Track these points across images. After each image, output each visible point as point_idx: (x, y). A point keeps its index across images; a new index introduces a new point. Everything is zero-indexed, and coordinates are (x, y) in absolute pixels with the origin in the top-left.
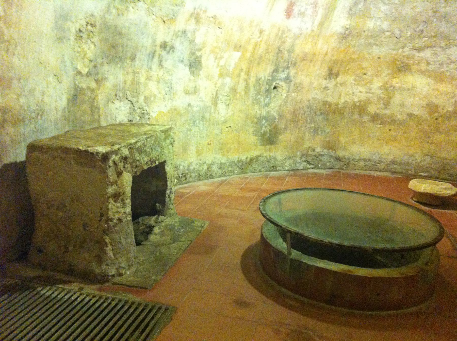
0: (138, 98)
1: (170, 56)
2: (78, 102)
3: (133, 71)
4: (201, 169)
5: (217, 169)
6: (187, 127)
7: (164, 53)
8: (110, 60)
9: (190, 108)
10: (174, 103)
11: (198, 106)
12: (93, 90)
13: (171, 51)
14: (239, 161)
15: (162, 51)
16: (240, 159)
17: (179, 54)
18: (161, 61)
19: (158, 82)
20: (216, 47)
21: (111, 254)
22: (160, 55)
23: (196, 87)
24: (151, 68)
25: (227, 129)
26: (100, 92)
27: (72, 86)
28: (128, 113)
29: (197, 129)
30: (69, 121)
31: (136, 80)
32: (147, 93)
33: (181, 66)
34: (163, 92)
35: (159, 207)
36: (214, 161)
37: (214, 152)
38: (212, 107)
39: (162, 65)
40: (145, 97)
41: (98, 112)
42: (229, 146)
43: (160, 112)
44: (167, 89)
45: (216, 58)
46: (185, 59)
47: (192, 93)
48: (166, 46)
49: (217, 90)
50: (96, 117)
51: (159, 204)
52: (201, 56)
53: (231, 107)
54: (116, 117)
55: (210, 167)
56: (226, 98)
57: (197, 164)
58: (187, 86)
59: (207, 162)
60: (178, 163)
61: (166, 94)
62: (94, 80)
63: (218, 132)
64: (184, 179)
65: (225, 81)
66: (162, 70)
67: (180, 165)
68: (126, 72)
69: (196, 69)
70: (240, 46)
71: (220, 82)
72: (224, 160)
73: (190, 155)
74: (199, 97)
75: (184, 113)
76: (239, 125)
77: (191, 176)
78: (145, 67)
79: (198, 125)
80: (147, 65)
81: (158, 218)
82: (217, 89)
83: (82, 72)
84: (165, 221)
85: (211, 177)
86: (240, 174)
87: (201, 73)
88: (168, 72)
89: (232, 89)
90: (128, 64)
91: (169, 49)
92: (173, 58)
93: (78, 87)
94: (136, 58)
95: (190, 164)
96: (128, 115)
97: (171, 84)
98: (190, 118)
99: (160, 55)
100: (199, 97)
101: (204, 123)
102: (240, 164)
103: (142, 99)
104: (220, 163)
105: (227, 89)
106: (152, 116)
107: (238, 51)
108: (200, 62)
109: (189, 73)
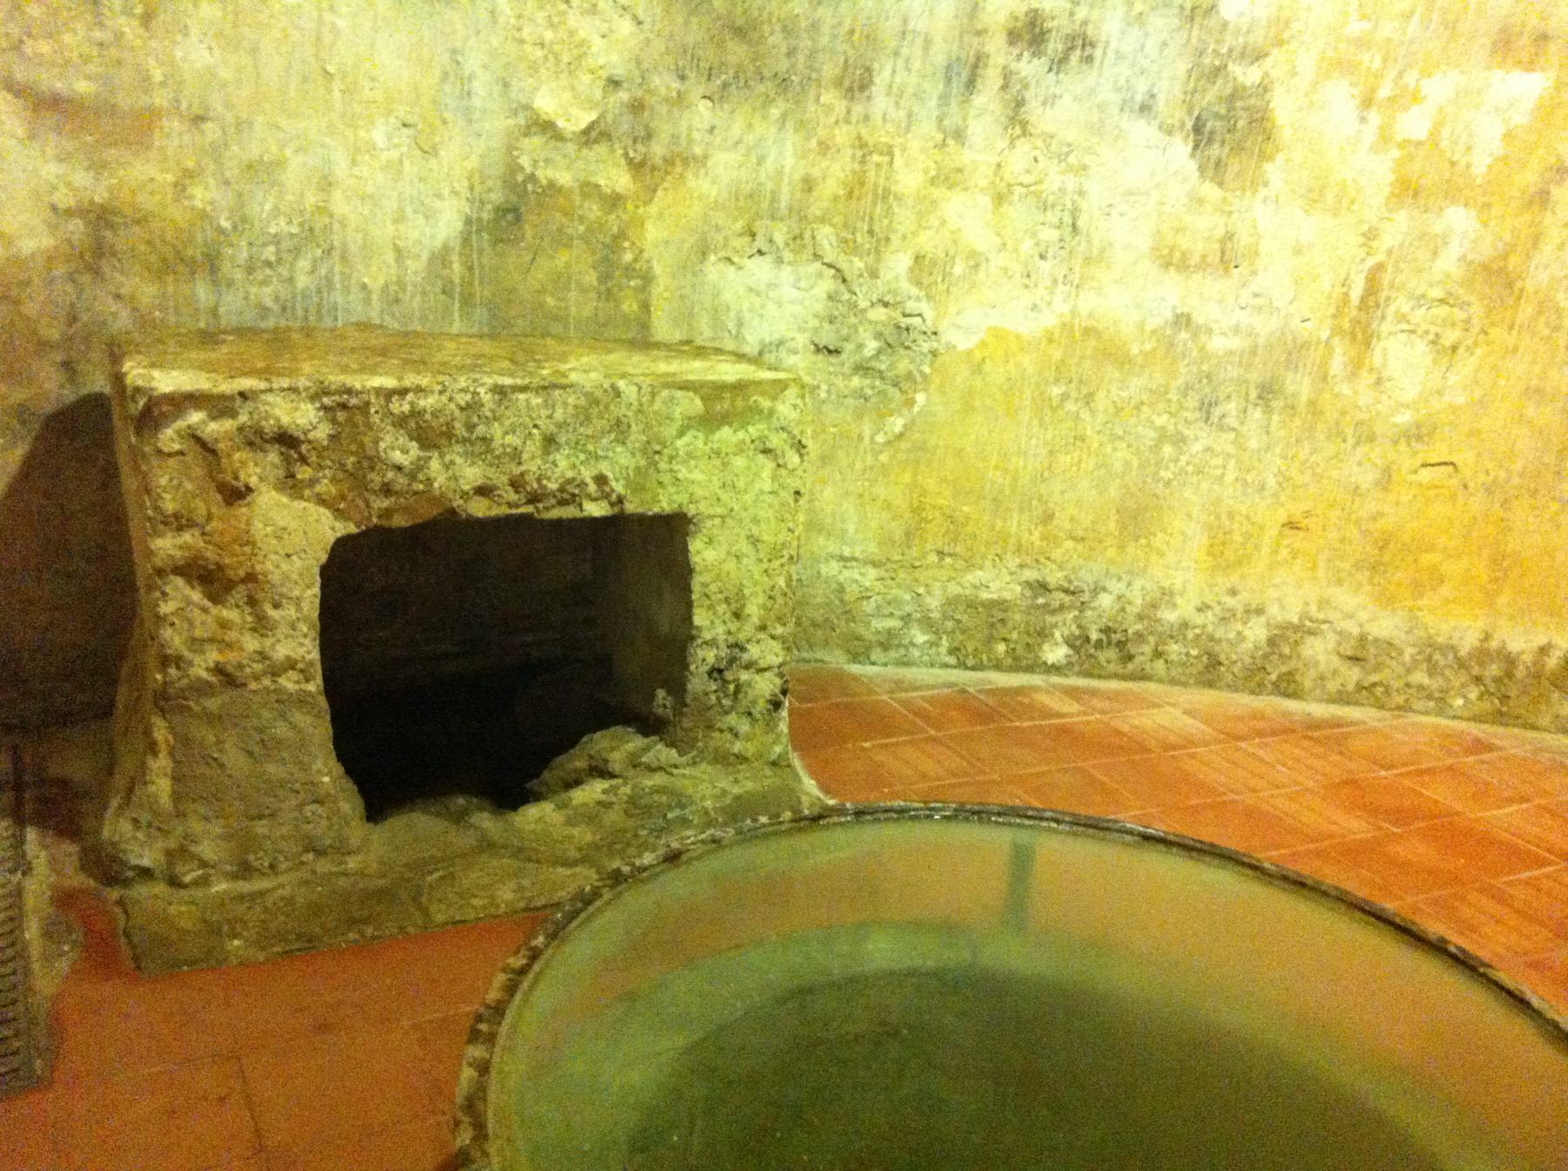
0: (878, 260)
1: (1073, 83)
2: (529, 234)
3: (859, 138)
4: (1229, 632)
5: (1336, 658)
6: (1160, 421)
7: (1030, 67)
8: (725, 86)
9: (1184, 335)
10: (1087, 303)
11: (1236, 330)
12: (614, 201)
13: (1075, 57)
14: (1482, 654)
15: (1020, 56)
16: (1494, 644)
17: (1124, 71)
18: (1020, 103)
19: (1000, 199)
20: (1361, 43)
21: (161, 786)
22: (1007, 76)
23: (1229, 237)
24: (959, 135)
25: (1425, 475)
26: (653, 209)
27: (498, 170)
28: (816, 316)
29: (1225, 443)
30: (467, 301)
31: (871, 176)
32: (928, 242)
33: (1142, 130)
34: (1027, 247)
35: (665, 706)
36: (1321, 616)
37: (1321, 573)
38: (1338, 350)
39: (1024, 125)
40: (918, 258)
41: (643, 289)
42: (1426, 559)
43: (998, 334)
44: (1050, 235)
45: (1367, 102)
46: (1161, 98)
47: (1204, 264)
48: (1043, 33)
49: (1380, 267)
50: (630, 306)
51: (669, 692)
52: (1264, 88)
53: (1466, 366)
54: (740, 324)
55: (1284, 638)
56: (1442, 311)
57: (1208, 607)
58: (1180, 230)
59: (1274, 611)
60: (1090, 579)
61: (1042, 257)
62: (623, 162)
63: (1366, 478)
64: (1112, 653)
65: (1438, 227)
66: (1023, 146)
67: (1098, 589)
68: (813, 144)
69: (1238, 149)
70: (1543, 38)
71: (1398, 228)
72: (1385, 626)
73: (1162, 554)
74: (1253, 288)
75: (1146, 355)
76: (1518, 466)
77: (1158, 654)
78: (926, 127)
79: (1232, 421)
80: (940, 120)
81: (646, 749)
82: (1380, 257)
83: (561, 123)
84: (675, 771)
85: (1288, 686)
86: (1476, 719)
87: (1272, 170)
88: (1062, 157)
89: (1486, 268)
90: (829, 109)
91: (1060, 47)
92: (1092, 92)
93: (532, 178)
94: (871, 82)
95: (1167, 596)
96: (813, 323)
97: (1075, 212)
98: (1180, 382)
99: (1007, 76)
100: (1253, 288)
101: (1275, 417)
102: (1494, 670)
103: (897, 264)
104: (1356, 631)
105: (1448, 263)
106: (951, 347)
107: (1530, 66)
108: (1261, 122)
109: (1192, 166)
